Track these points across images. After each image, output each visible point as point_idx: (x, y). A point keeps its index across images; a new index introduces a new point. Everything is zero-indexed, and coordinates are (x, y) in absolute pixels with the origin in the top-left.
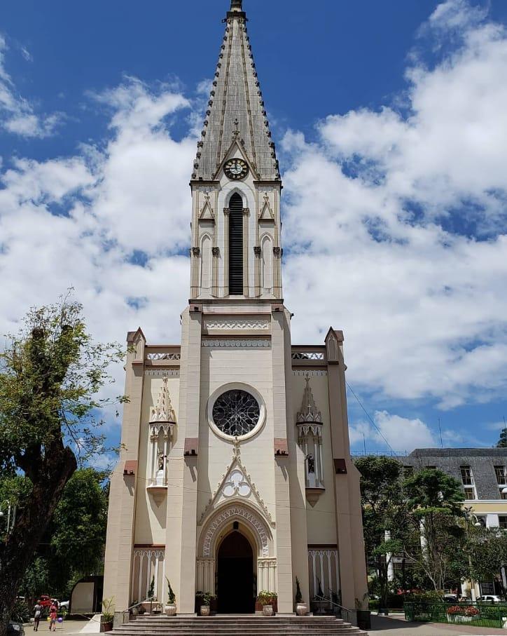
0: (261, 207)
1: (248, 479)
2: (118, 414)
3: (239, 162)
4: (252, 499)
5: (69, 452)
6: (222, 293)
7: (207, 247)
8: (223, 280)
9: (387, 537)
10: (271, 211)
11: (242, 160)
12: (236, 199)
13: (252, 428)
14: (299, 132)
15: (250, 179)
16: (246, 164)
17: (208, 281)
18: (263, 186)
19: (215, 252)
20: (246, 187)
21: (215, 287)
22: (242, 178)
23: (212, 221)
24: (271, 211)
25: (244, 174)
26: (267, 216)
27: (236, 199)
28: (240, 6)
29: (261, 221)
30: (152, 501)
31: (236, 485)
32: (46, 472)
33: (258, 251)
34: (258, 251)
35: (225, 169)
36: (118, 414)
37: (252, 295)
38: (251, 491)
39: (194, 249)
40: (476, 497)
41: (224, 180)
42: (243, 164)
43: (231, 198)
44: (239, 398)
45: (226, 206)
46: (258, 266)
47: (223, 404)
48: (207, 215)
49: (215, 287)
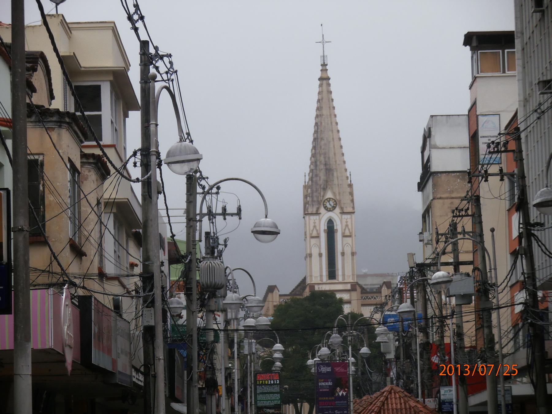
0: (344, 228)
2: (322, 25)
3: (331, 200)
5: (144, 330)
6: (325, 279)
7: (315, 252)
9: (72, 396)
10: (349, 230)
11: (333, 199)
12: (330, 222)
14: (310, 293)
15: (338, 210)
16: (335, 201)
18: (345, 215)
19: (320, 255)
20: (335, 215)
21: (321, 276)
22: (333, 210)
23: (318, 237)
24: (349, 230)
25: (334, 208)
26: (347, 233)
27: (330, 222)
29: (344, 236)
32: (472, 363)
33: (343, 254)
34: (343, 254)
35: (324, 205)
36: (322, 25)
38: (503, 348)
39: (309, 254)
41: (322, 210)
42: (333, 201)
43: (328, 222)
49: (321, 276)
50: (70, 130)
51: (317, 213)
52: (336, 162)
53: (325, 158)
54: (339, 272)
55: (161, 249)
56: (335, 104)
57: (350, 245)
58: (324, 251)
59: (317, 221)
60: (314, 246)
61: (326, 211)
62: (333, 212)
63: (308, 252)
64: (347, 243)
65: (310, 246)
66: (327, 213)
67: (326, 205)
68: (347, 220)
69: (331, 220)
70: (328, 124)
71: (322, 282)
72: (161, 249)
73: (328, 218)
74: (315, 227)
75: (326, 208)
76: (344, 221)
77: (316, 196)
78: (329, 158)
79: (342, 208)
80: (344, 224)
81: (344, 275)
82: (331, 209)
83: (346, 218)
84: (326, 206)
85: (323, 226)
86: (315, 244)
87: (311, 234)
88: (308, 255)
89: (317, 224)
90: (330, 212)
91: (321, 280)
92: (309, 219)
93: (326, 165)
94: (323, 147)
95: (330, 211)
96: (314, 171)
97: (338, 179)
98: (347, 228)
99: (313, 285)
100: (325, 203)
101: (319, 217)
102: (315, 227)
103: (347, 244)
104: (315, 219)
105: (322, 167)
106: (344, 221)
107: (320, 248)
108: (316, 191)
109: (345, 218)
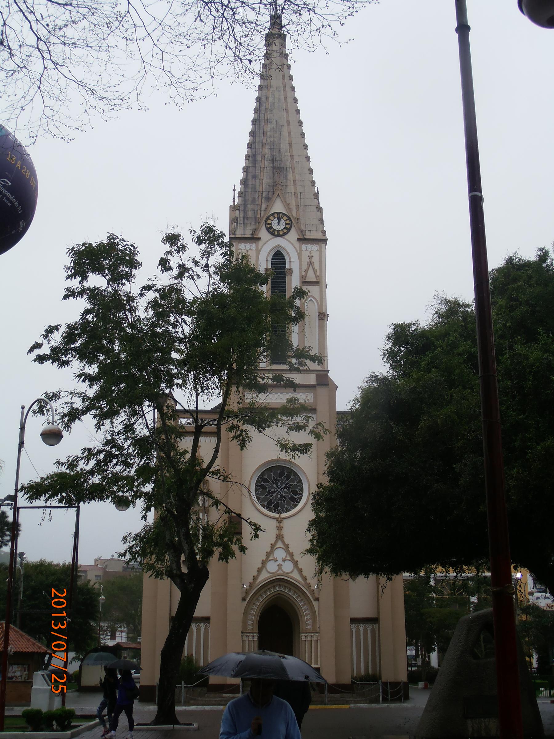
4: (296, 576)
15: (293, 235)
35: (266, 224)
44: (282, 475)
45: (267, 265)
47: (266, 481)
51: (254, 239)
52: (292, 156)
53: (272, 150)
61: (271, 236)
68: (310, 252)
70: (279, 100)
76: (305, 256)
77: (252, 210)
83: (310, 250)
90: (279, 238)
93: (273, 161)
95: (278, 235)
100: (288, 222)
104: (248, 249)
106: (305, 256)
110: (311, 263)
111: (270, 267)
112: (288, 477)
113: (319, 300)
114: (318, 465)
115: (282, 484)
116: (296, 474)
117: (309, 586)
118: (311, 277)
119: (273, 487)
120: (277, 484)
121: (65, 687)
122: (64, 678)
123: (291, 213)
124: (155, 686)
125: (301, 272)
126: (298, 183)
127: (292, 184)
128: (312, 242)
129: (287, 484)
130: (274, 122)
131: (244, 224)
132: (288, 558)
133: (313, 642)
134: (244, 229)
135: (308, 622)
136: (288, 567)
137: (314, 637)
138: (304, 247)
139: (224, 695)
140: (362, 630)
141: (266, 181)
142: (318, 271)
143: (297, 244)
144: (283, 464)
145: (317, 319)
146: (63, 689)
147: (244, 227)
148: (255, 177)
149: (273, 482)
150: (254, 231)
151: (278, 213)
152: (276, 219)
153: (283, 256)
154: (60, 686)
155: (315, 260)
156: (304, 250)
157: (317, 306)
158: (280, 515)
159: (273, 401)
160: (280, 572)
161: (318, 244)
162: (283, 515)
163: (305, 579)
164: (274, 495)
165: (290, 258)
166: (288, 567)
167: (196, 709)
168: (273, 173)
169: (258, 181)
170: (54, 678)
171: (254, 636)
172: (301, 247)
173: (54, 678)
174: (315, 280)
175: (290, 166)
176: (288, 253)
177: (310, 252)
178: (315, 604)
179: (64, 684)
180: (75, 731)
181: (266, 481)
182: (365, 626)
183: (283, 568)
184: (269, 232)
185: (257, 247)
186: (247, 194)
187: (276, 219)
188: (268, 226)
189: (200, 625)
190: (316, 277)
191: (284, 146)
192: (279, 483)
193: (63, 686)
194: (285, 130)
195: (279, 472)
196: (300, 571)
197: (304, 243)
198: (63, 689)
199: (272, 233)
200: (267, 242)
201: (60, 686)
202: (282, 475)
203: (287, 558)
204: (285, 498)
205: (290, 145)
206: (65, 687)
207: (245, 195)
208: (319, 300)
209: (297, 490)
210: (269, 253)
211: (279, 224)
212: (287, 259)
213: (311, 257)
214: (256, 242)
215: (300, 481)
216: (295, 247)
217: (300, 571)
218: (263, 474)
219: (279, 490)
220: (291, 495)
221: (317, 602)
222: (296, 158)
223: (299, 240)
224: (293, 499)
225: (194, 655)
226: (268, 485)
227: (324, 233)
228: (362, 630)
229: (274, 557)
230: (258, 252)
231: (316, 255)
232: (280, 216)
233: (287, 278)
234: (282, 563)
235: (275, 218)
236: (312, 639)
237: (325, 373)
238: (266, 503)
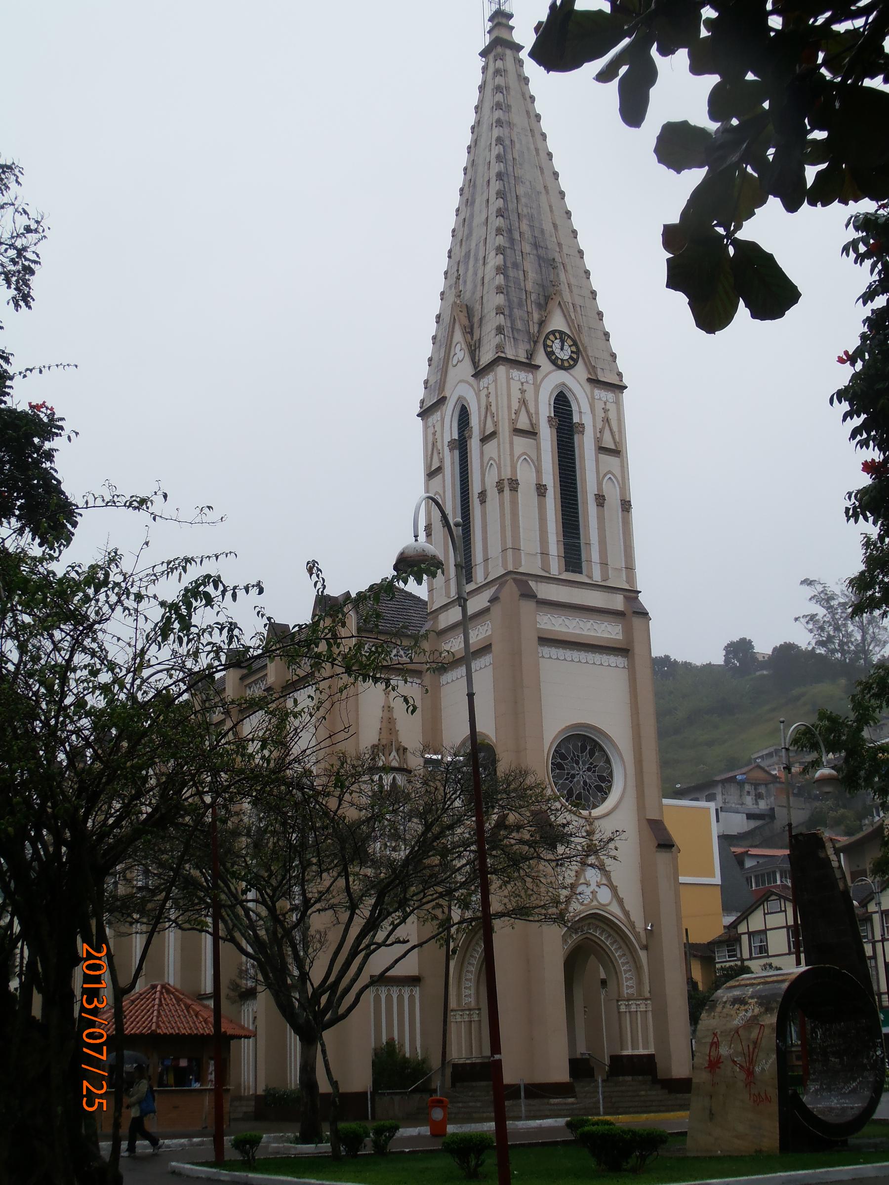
1: (609, 878)
4: (615, 909)
6: (555, 567)
7: (526, 476)
8: (554, 548)
12: (562, 404)
13: (604, 800)
15: (580, 370)
17: (529, 542)
19: (541, 490)
21: (545, 554)
23: (532, 433)
27: (562, 404)
28: (774, 873)
30: (872, 972)
31: (593, 886)
33: (600, 500)
35: (545, 346)
37: (597, 577)
40: (868, 871)
41: (541, 359)
44: (583, 748)
45: (550, 413)
46: (601, 519)
47: (563, 757)
48: (523, 423)
50: (245, 1086)
51: (530, 366)
52: (560, 245)
53: (532, 227)
54: (593, 553)
55: (753, 824)
56: (539, 107)
57: (532, 461)
58: (550, 478)
59: (529, 389)
60: (520, 461)
61: (553, 367)
62: (569, 373)
63: (507, 474)
64: (610, 472)
65: (512, 454)
66: (554, 371)
67: (551, 347)
68: (605, 403)
69: (565, 397)
70: (528, 149)
71: (548, 575)
72: (753, 824)
73: (557, 386)
74: (523, 402)
75: (553, 357)
76: (599, 406)
77: (521, 319)
78: (542, 231)
79: (591, 368)
80: (600, 414)
81: (604, 564)
82: (566, 364)
83: (604, 399)
84: (553, 353)
85: (545, 410)
86: (525, 454)
87: (514, 422)
88: (506, 482)
89: (529, 396)
90: (562, 373)
91: (545, 567)
92: (509, 379)
93: (536, 246)
94: (523, 200)
95: (561, 367)
96: (508, 251)
97: (571, 291)
98: (523, 409)
99: (524, 578)
100: (549, 343)
101: (535, 379)
102: (523, 402)
103: (609, 476)
104: (523, 380)
105: (527, 248)
106: (599, 406)
107: (539, 471)
108: (520, 305)
109: (600, 399)
110: (607, 420)
111: (553, 415)
112: (592, 754)
113: (620, 479)
114: (357, 711)
115: (584, 763)
116: (602, 749)
117: (633, 925)
118: (608, 443)
119: (573, 768)
120: (577, 764)
121: (105, 1102)
122: (102, 1088)
123: (579, 336)
124: (366, 1093)
125: (595, 433)
126: (575, 290)
127: (568, 290)
128: (609, 388)
129: (591, 764)
130: (528, 183)
131: (514, 338)
132: (604, 881)
133: (639, 1013)
134: (515, 348)
135: (628, 983)
136: (604, 896)
137: (641, 1006)
138: (597, 392)
139: (552, 1101)
140: (406, 997)
141: (531, 275)
142: (534, 416)
143: (587, 387)
144: (586, 732)
145: (620, 510)
146: (101, 1104)
147: (515, 345)
148: (515, 265)
149: (572, 759)
150: (531, 355)
151: (561, 332)
152: (558, 341)
153: (568, 402)
154: (97, 1101)
155: (612, 415)
156: (596, 397)
157: (618, 489)
158: (590, 813)
159: (571, 631)
160: (595, 903)
161: (614, 392)
162: (595, 812)
163: (627, 914)
164: (575, 780)
165: (579, 407)
166: (604, 896)
167: (556, 1125)
168: (540, 266)
169: (521, 273)
170: (87, 1087)
171: (639, 1005)
172: (592, 393)
173: (87, 1087)
174: (613, 447)
175: (560, 261)
176: (576, 399)
177: (605, 403)
178: (643, 955)
179: (101, 1096)
180: (258, 1178)
181: (563, 757)
182: (400, 990)
183: (599, 896)
184: (549, 359)
185: (535, 379)
186: (509, 289)
187: (558, 341)
188: (549, 349)
189: (414, 989)
190: (615, 443)
191: (548, 227)
192: (581, 763)
193: (101, 1101)
194: (543, 198)
195: (580, 744)
196: (620, 902)
197: (597, 387)
198: (101, 1104)
199: (554, 362)
200: (575, 378)
201: (97, 1101)
202: (583, 748)
203: (602, 882)
204: (590, 786)
205: (555, 226)
206: (105, 1102)
207: (508, 292)
208: (620, 479)
209: (605, 775)
210: (551, 393)
211: (562, 349)
212: (574, 407)
213: (606, 411)
214: (617, 391)
215: (608, 761)
216: (585, 391)
217: (620, 902)
218: (559, 746)
219: (581, 773)
220: (597, 782)
221: (645, 952)
222: (565, 250)
223: (589, 380)
224: (599, 789)
225: (396, 1038)
226: (566, 764)
227: (620, 375)
228: (406, 997)
229: (585, 878)
230: (537, 387)
231: (612, 407)
232: (562, 336)
233: (576, 437)
234: (597, 889)
235: (556, 339)
236: (638, 1009)
237: (634, 595)
238: (599, 794)
